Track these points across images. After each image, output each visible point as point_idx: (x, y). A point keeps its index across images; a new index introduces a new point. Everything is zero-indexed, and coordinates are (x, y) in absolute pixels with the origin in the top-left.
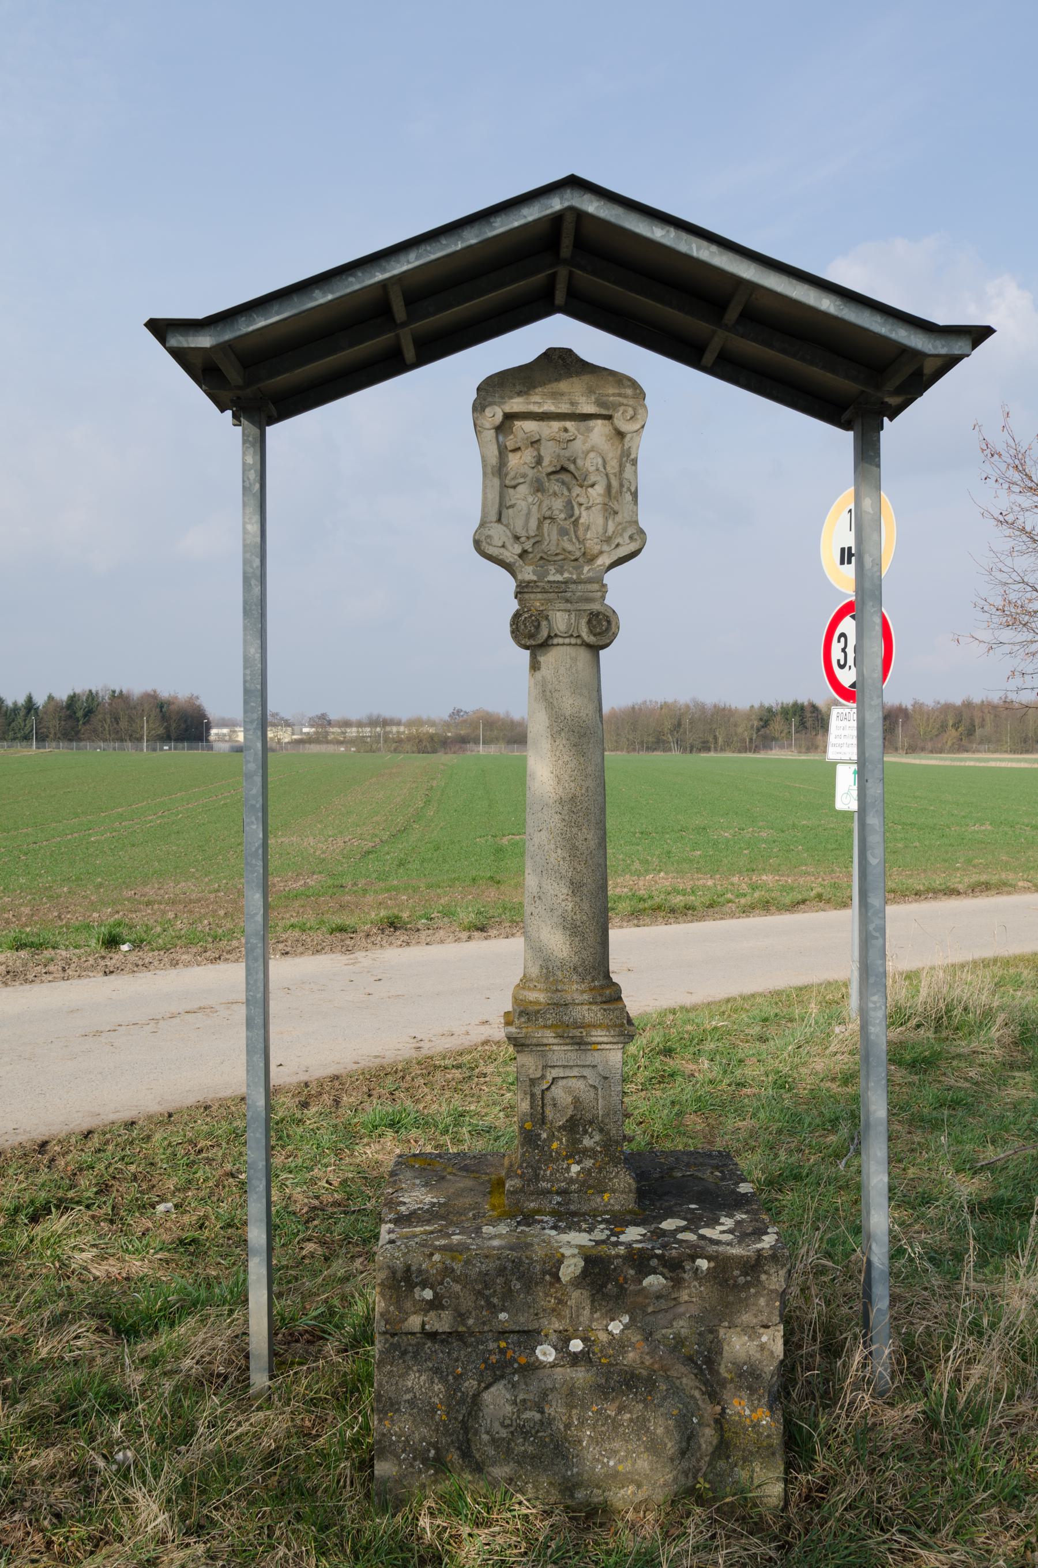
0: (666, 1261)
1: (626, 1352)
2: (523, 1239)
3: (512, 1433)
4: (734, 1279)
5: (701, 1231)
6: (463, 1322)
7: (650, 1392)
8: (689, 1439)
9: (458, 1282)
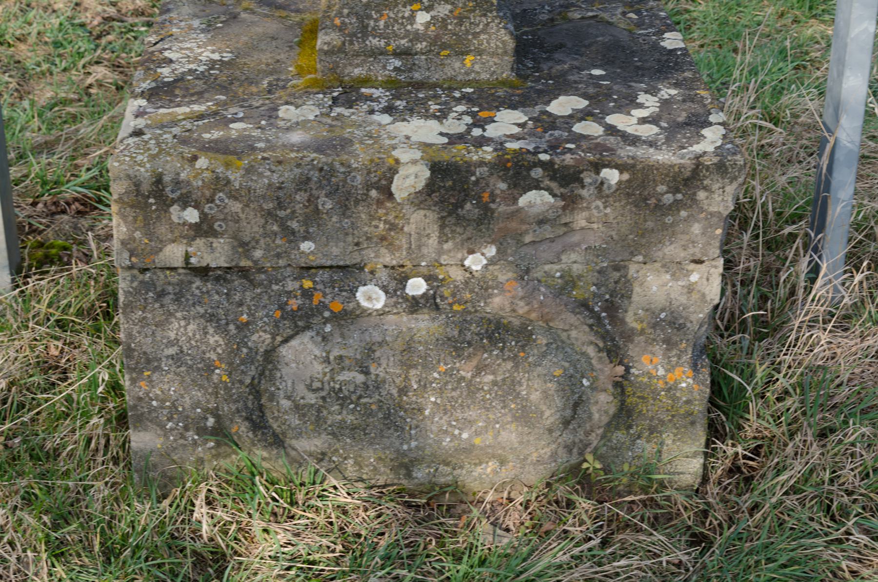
0: (555, 171)
1: (490, 296)
2: (338, 132)
3: (323, 398)
4: (659, 198)
5: (611, 119)
6: (247, 254)
7: (523, 346)
8: (576, 405)
9: (236, 199)
